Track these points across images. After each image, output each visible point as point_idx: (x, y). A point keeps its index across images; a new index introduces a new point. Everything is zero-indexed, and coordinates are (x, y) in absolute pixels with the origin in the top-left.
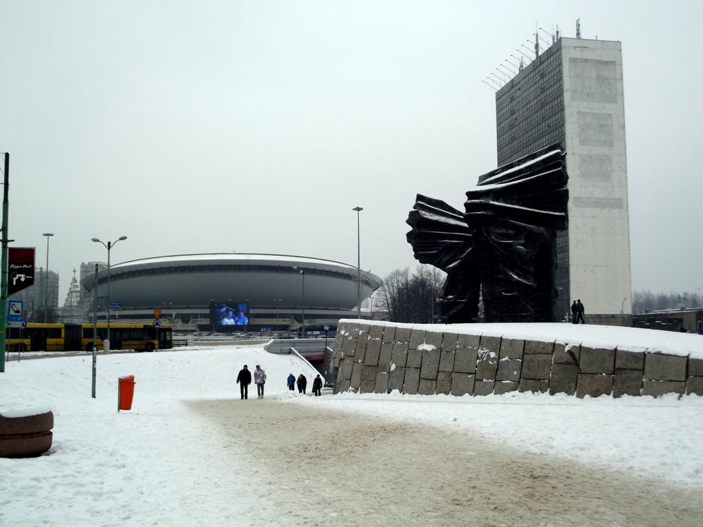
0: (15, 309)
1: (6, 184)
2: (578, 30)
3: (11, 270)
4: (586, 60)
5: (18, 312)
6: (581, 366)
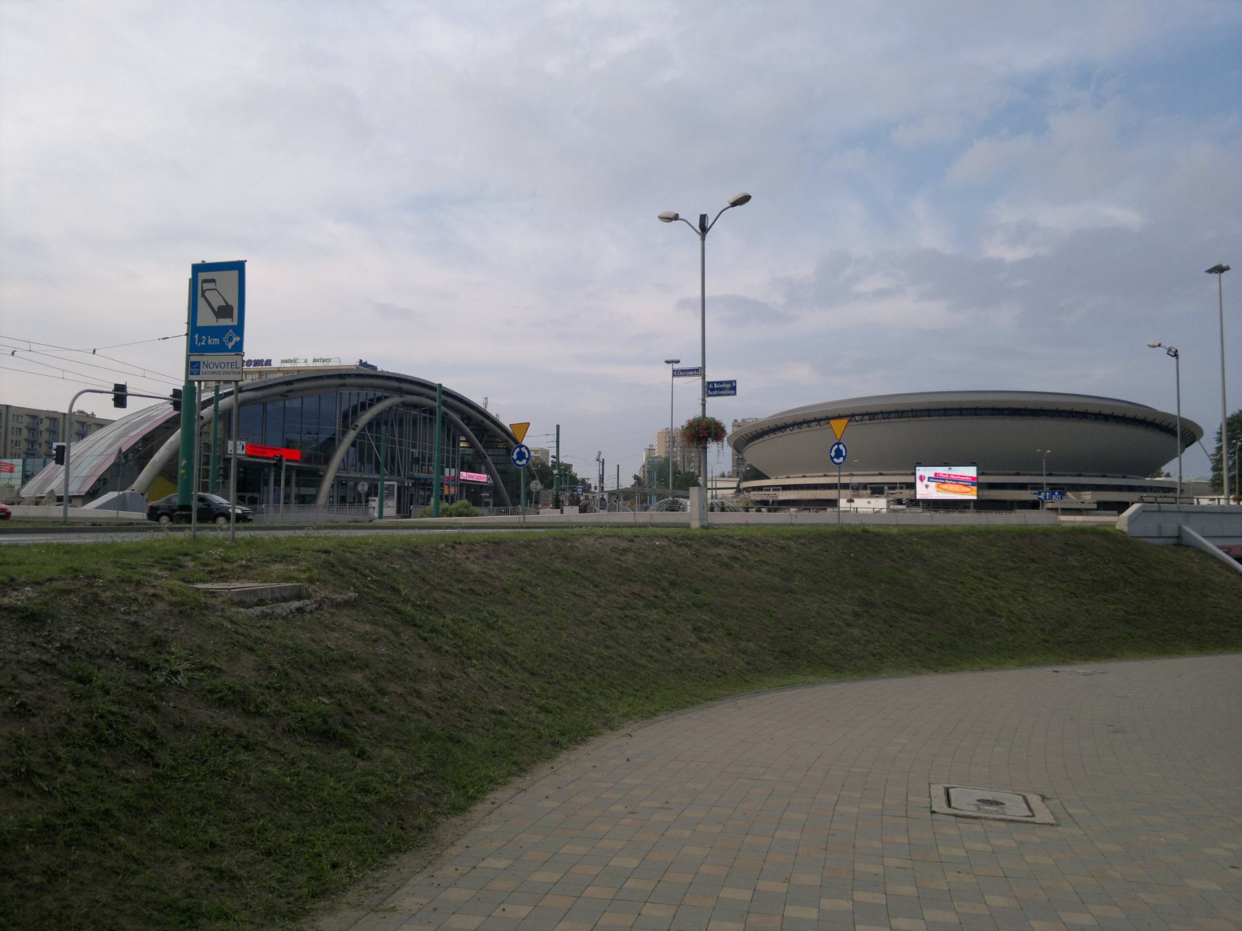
0: (217, 302)
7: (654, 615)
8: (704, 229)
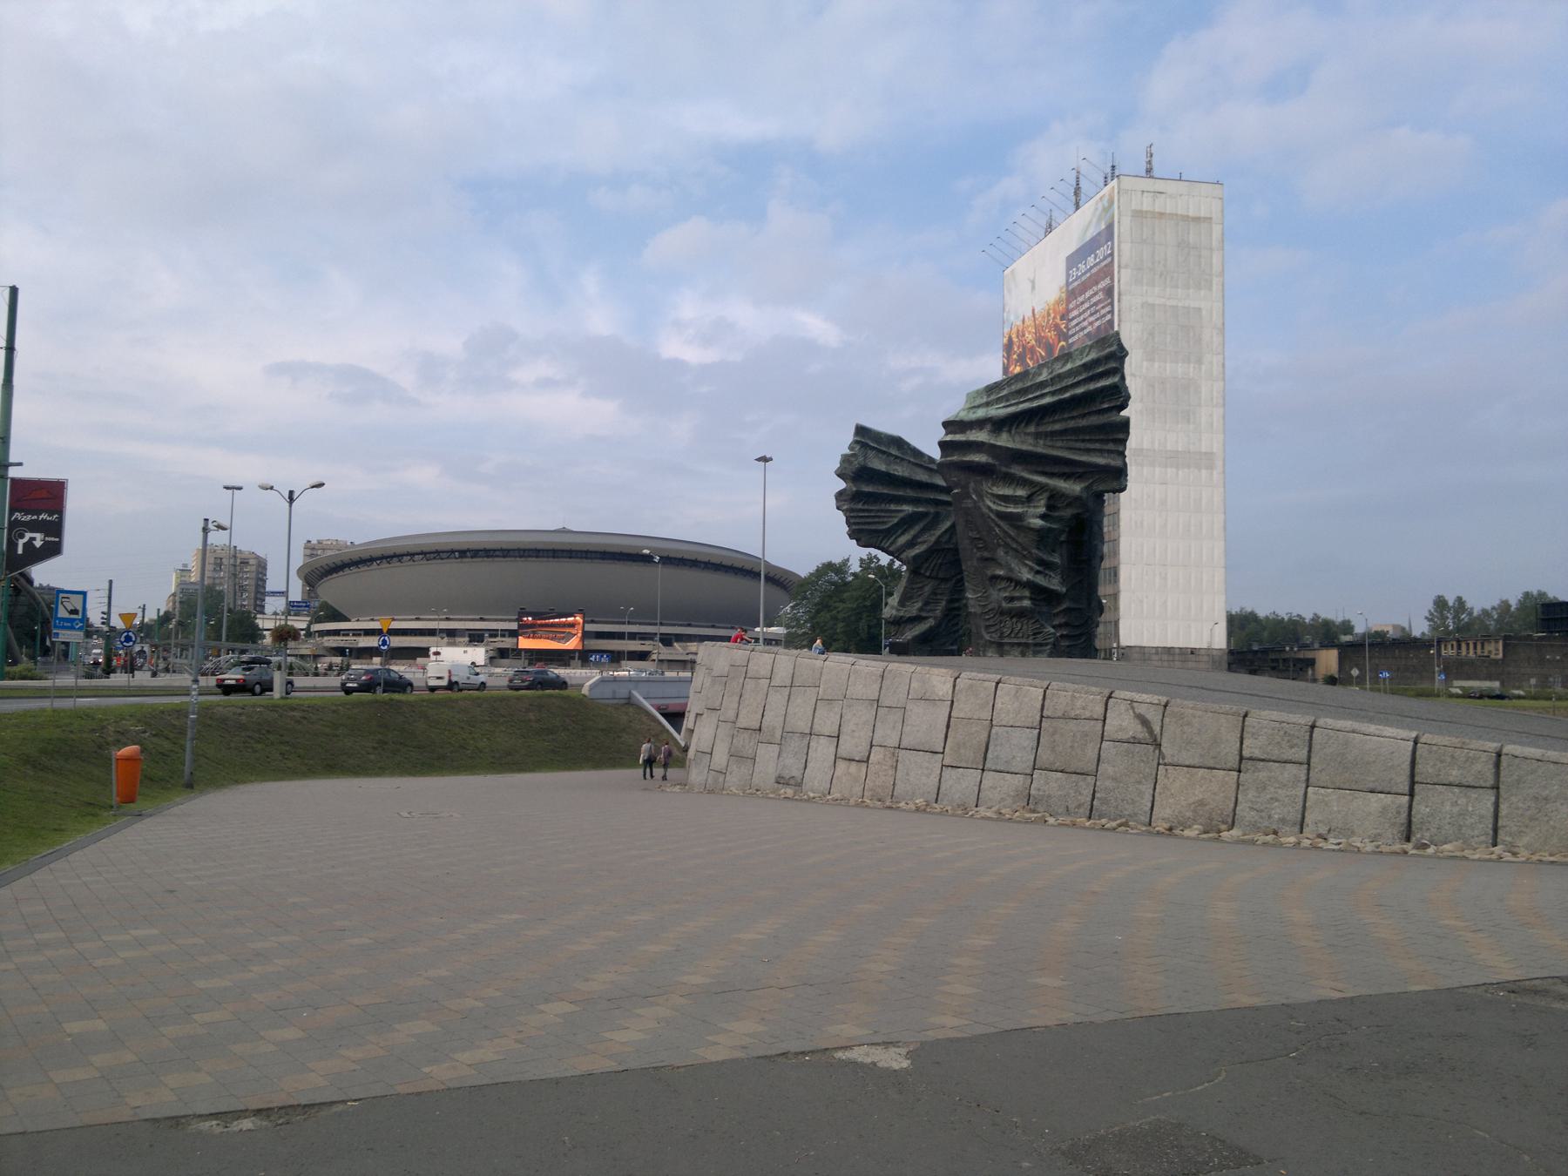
0: (70, 607)
1: (10, 349)
2: (1149, 162)
3: (13, 525)
4: (1162, 215)
5: (75, 612)
6: (1166, 748)
7: (259, 746)
8: (291, 498)
